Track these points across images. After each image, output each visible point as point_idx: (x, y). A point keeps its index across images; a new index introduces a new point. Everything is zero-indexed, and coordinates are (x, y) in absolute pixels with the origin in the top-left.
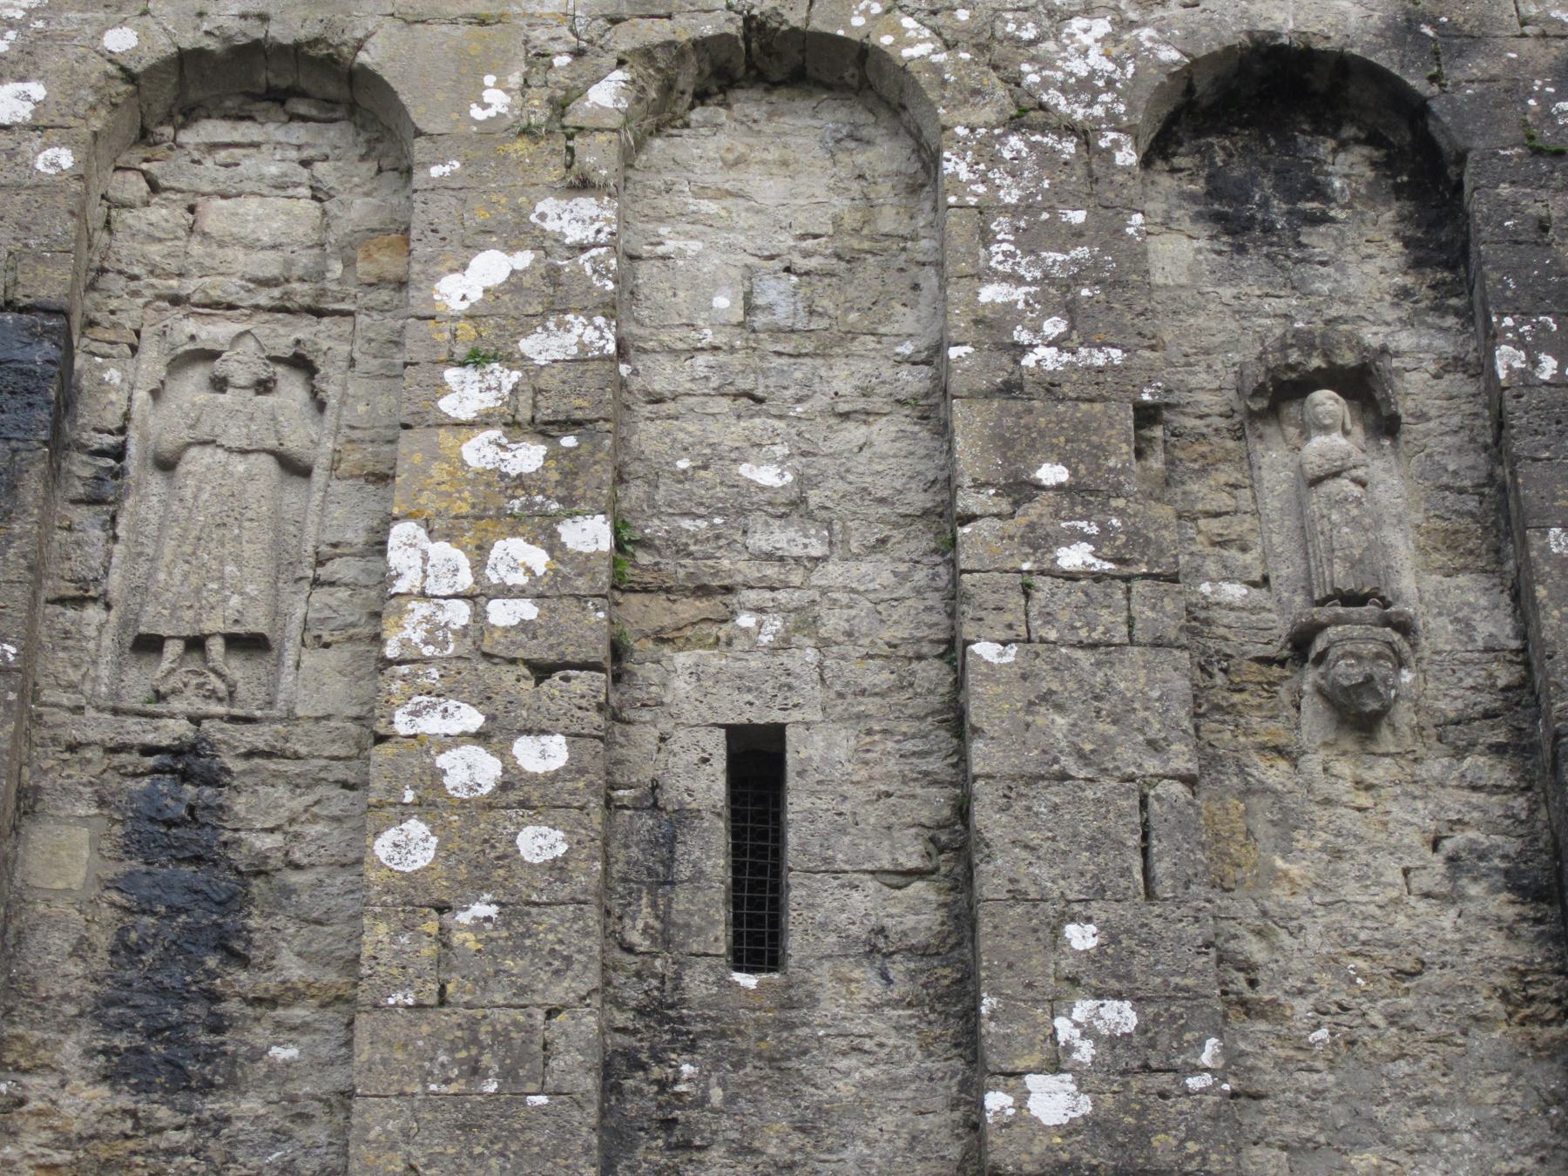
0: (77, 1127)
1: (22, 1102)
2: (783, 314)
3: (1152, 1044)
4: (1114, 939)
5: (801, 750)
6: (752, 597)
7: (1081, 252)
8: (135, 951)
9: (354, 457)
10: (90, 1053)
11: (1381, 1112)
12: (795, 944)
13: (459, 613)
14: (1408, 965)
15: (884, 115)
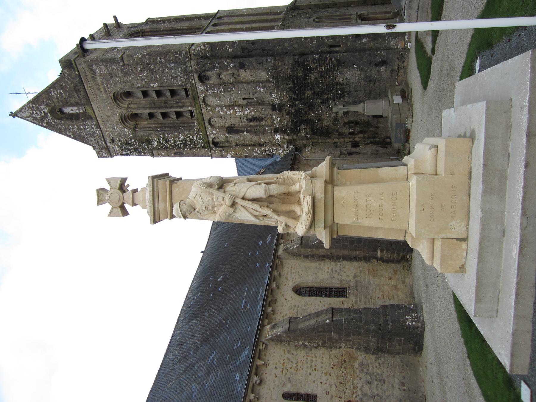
5: (244, 97)
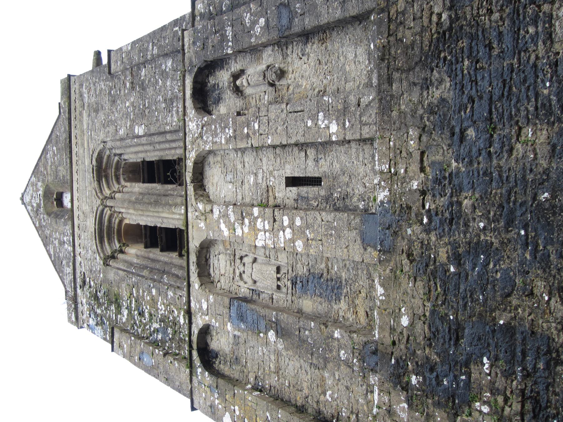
0: (347, 307)
1: (343, 316)
2: (231, 177)
3: (325, 109)
4: (310, 117)
6: (268, 182)
7: (218, 126)
8: (321, 294)
9: (253, 250)
10: (336, 303)
11: (340, 66)
12: (316, 175)
13: (267, 234)
14: (318, 62)
15: (206, 159)
